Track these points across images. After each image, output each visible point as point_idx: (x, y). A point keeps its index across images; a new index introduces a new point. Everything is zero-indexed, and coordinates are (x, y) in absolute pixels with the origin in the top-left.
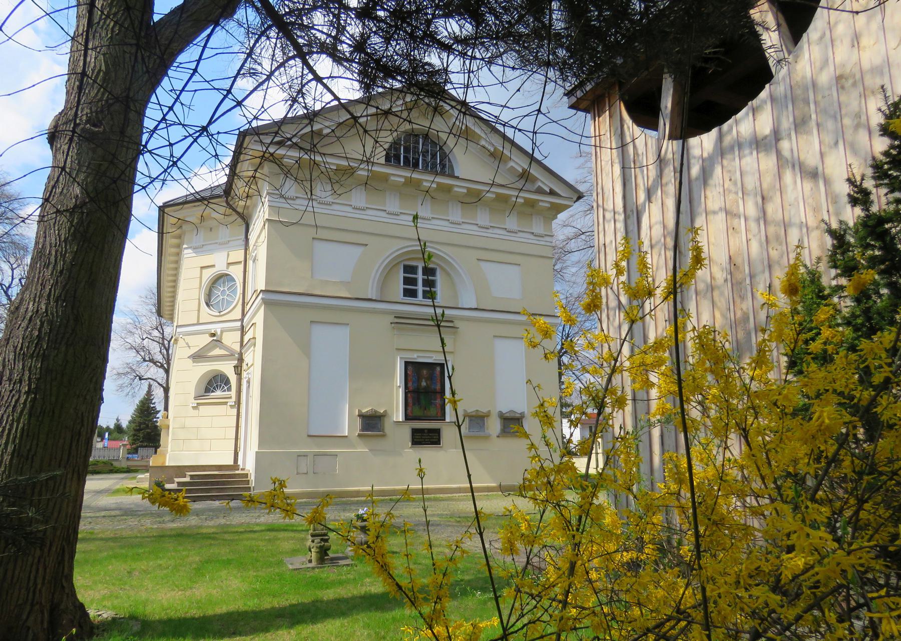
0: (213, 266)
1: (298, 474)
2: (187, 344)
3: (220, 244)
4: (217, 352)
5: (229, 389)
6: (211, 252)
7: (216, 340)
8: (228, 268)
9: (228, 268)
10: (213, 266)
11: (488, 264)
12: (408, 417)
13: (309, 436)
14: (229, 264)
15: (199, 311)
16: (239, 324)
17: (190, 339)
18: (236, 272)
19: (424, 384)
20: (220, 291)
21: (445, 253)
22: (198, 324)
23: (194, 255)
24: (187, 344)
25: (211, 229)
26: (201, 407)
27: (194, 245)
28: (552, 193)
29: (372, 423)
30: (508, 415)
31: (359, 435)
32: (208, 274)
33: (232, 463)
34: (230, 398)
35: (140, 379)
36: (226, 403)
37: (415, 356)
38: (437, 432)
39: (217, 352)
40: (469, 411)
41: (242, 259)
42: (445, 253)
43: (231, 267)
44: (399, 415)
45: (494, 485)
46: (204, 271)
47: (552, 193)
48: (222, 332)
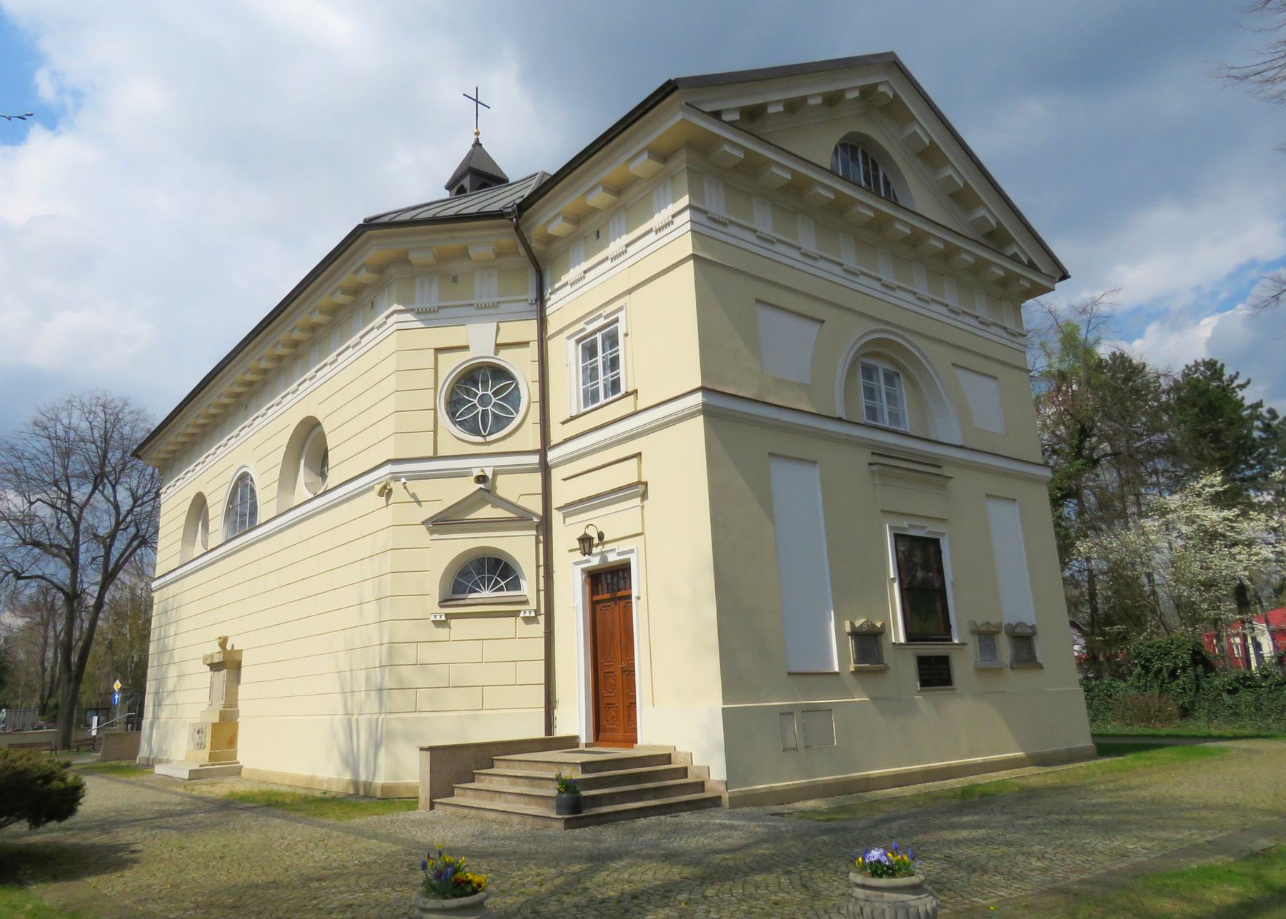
0: (466, 348)
1: (785, 750)
2: (413, 495)
3: (479, 307)
4: (487, 512)
5: (515, 585)
6: (459, 322)
7: (486, 488)
8: (496, 353)
9: (496, 353)
10: (466, 348)
11: (970, 376)
12: (910, 637)
13: (790, 674)
14: (499, 346)
15: (435, 432)
16: (535, 459)
17: (422, 488)
18: (522, 366)
19: (919, 574)
20: (484, 396)
21: (918, 350)
22: (435, 458)
23: (419, 324)
24: (413, 495)
25: (455, 279)
26: (453, 622)
27: (418, 305)
28: (1032, 266)
29: (868, 642)
30: (984, 629)
31: (858, 672)
32: (451, 365)
33: (540, 733)
34: (526, 602)
35: (18, 576)
36: (515, 614)
37: (905, 524)
38: (944, 661)
39: (487, 512)
40: (979, 622)
41: (535, 336)
42: (918, 350)
43: (504, 354)
44: (898, 634)
45: (1021, 754)
46: (442, 357)
47: (1032, 266)
48: (495, 474)
